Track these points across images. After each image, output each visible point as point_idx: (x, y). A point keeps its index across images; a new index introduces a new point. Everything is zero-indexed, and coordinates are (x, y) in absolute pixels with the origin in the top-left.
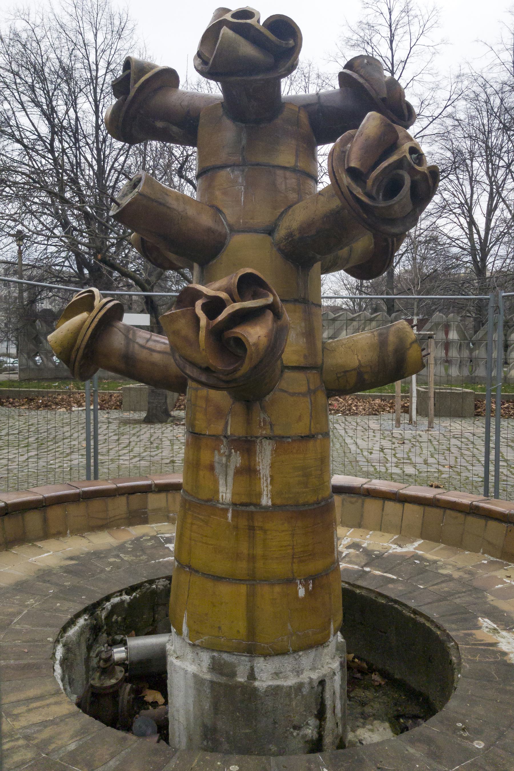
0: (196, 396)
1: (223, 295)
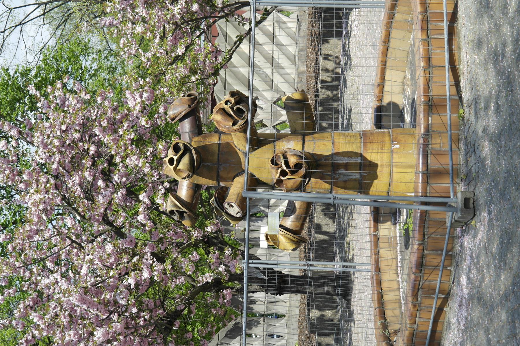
0: (315, 188)
1: (280, 170)
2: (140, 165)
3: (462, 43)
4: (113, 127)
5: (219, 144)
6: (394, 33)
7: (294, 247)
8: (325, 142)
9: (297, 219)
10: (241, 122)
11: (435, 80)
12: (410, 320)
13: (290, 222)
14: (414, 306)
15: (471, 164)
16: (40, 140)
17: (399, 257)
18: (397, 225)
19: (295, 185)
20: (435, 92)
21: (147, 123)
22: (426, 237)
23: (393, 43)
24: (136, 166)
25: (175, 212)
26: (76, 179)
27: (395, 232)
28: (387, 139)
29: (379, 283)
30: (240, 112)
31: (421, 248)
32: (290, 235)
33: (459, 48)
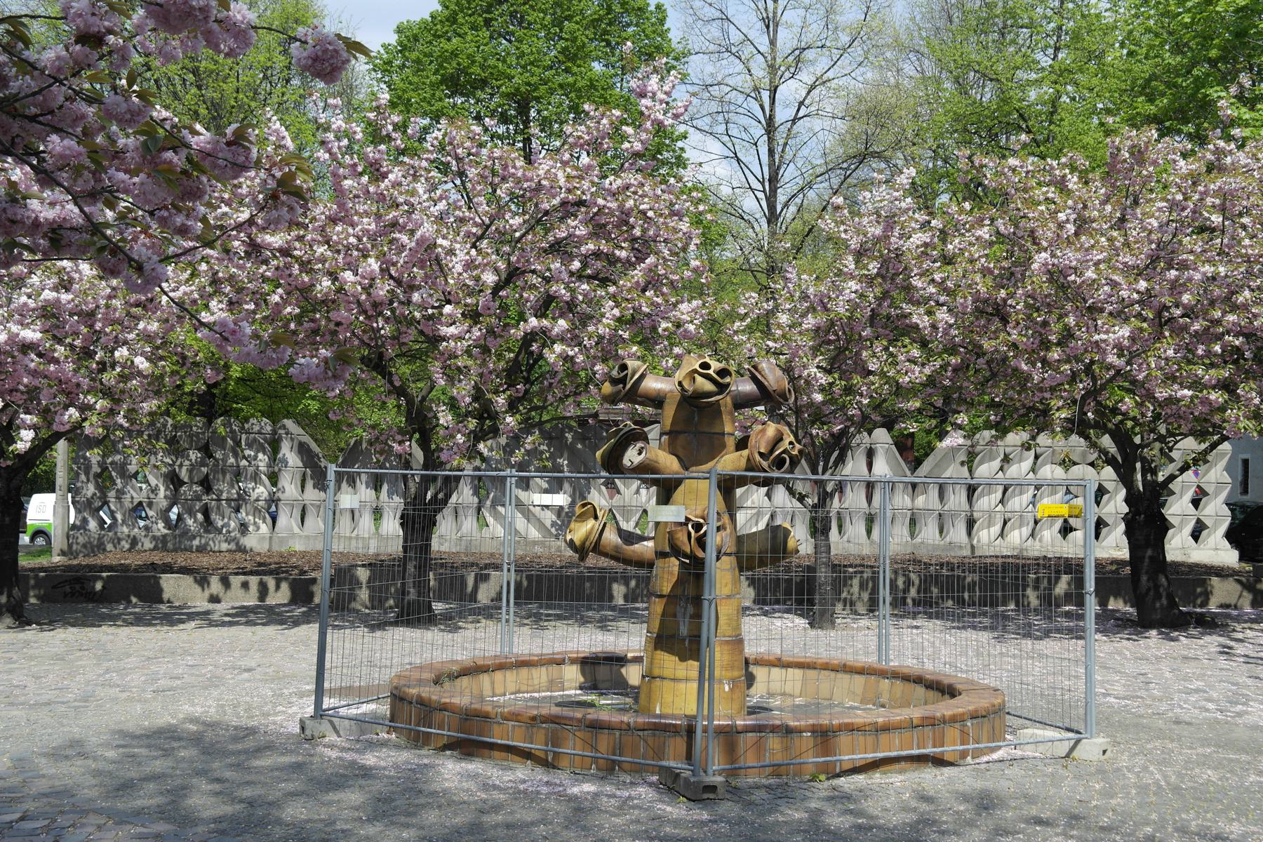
2: (604, 320)
3: (908, 775)
4: (652, 282)
5: (723, 434)
6: (859, 680)
7: (577, 543)
8: (730, 586)
9: (617, 548)
10: (765, 464)
11: (860, 738)
12: (509, 713)
13: (611, 537)
14: (534, 718)
15: (757, 792)
16: (632, 181)
17: (536, 695)
18: (579, 692)
19: (679, 544)
20: (844, 740)
21: (665, 330)
22: (641, 733)
23: (844, 678)
24: (603, 315)
26: (582, 231)
27: (571, 689)
28: (736, 674)
29: (501, 667)
30: (779, 463)
31: (624, 727)
32: (594, 537)
33: (900, 772)
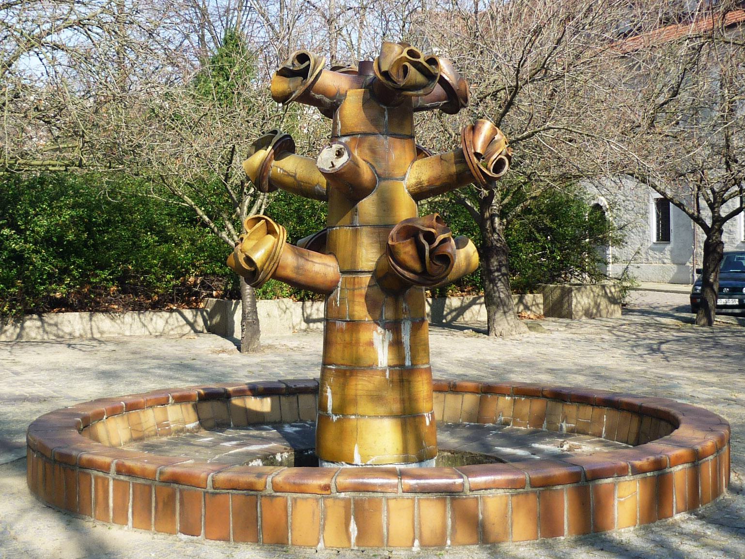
25: (307, 63)
